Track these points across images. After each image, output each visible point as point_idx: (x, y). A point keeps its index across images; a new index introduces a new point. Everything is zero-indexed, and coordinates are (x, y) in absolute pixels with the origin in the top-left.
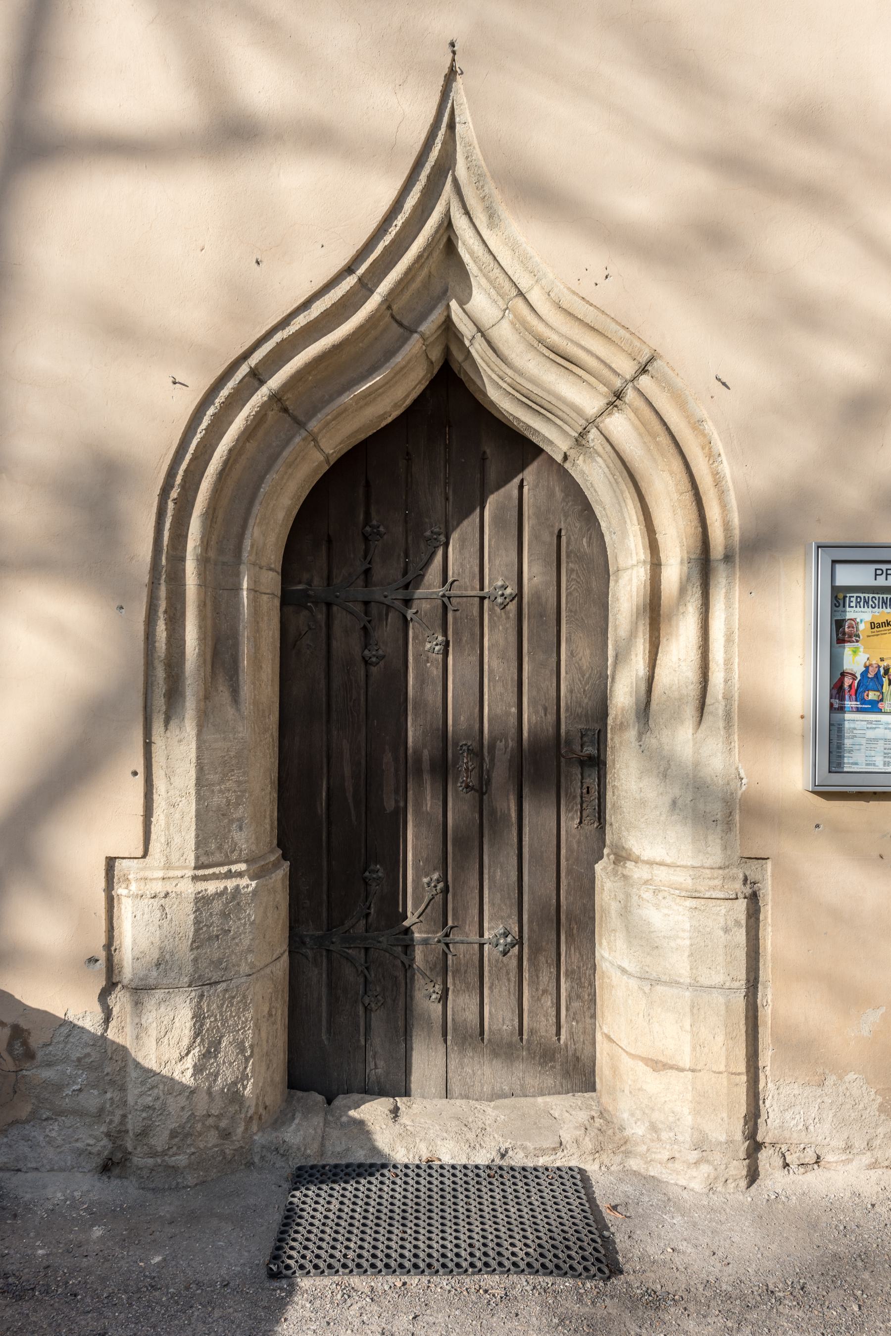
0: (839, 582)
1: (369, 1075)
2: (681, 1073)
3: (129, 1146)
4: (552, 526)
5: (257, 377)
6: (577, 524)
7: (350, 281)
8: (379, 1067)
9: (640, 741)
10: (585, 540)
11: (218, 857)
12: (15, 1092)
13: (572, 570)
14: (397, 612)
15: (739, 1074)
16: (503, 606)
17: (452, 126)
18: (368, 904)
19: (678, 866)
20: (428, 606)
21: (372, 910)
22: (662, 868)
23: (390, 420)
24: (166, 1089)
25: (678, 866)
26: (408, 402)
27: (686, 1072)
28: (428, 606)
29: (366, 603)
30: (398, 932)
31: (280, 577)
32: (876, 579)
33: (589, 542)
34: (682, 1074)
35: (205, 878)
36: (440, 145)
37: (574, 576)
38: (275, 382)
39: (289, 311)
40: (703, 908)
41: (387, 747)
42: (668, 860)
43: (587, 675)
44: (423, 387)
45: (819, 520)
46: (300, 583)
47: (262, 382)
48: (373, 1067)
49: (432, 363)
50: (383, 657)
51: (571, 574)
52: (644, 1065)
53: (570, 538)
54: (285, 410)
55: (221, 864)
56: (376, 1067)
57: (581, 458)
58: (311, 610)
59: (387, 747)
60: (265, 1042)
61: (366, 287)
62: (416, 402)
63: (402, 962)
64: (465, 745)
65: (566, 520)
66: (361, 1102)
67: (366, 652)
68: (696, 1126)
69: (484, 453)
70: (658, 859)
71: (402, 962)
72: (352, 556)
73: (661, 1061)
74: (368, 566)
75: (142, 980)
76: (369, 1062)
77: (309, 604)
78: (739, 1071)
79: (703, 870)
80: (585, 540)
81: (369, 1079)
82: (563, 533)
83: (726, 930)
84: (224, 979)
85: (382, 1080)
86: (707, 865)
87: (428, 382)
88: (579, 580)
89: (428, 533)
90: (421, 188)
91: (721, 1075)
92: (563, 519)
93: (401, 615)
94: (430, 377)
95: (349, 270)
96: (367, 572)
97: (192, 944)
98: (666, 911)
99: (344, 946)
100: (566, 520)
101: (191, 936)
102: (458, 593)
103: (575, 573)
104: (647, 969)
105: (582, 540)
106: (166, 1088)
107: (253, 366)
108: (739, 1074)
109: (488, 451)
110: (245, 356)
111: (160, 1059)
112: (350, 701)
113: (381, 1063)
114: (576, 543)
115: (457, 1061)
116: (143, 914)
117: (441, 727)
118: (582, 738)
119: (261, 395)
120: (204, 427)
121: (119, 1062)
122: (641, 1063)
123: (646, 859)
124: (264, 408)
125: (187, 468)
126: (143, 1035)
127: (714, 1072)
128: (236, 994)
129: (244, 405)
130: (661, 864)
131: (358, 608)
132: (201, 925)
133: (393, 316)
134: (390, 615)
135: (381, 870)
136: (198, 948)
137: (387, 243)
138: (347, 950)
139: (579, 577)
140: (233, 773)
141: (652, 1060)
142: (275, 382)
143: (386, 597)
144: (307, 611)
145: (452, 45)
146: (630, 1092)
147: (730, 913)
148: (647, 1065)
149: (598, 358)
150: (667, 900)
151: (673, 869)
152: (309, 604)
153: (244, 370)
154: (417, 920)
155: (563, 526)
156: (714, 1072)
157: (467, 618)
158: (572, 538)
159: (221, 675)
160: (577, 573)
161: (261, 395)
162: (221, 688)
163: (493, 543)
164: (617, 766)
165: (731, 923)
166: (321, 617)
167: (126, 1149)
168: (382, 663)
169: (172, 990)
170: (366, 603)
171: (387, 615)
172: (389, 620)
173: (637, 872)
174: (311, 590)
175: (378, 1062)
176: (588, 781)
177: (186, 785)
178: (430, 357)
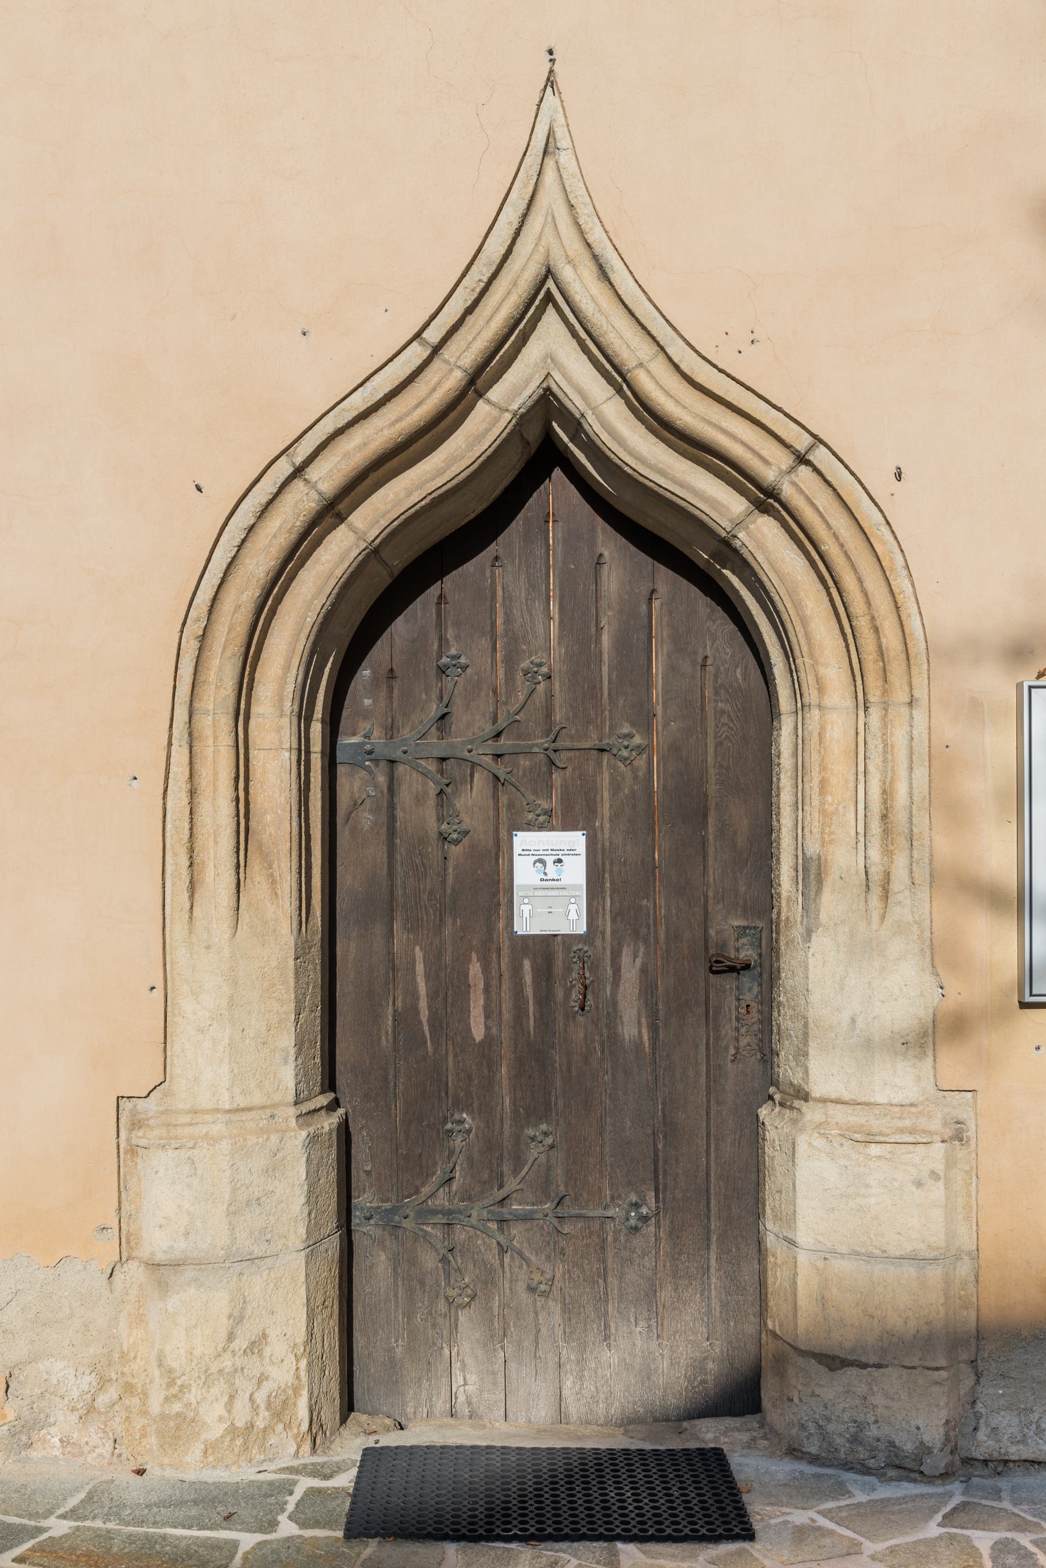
1: (456, 1393)
2: (863, 1370)
4: (695, 653)
6: (728, 650)
8: (469, 1382)
10: (739, 671)
13: (723, 712)
14: (486, 772)
18: (451, 1165)
19: (859, 1104)
20: (527, 763)
22: (839, 1106)
25: (859, 1104)
27: (869, 1369)
28: (527, 763)
30: (492, 1202)
33: (745, 674)
34: (865, 1372)
37: (725, 720)
40: (888, 1156)
41: (474, 956)
42: (846, 1096)
46: (354, 734)
48: (462, 1383)
49: (528, 444)
50: (466, 833)
51: (721, 716)
52: (816, 1364)
53: (719, 668)
56: (465, 1384)
58: (371, 772)
59: (474, 956)
63: (498, 1243)
65: (713, 644)
66: (525, 826)
67: (444, 826)
69: (601, 555)
71: (498, 1243)
72: (424, 697)
73: (839, 1357)
74: (446, 710)
75: (165, 1252)
77: (367, 763)
79: (890, 1108)
80: (739, 671)
82: (709, 662)
85: (474, 1400)
86: (895, 1101)
88: (731, 725)
92: (709, 643)
93: (491, 775)
94: (525, 458)
98: (843, 1162)
99: (420, 1221)
100: (713, 644)
101: (227, 1197)
102: (568, 744)
103: (726, 716)
105: (735, 670)
107: (297, 464)
109: (606, 553)
111: (191, 1353)
112: (424, 892)
113: (472, 1378)
114: (727, 675)
116: (167, 1169)
123: (818, 1095)
130: (838, 1102)
131: (432, 767)
134: (476, 776)
135: (469, 1119)
139: (732, 720)
140: (274, 989)
141: (826, 1356)
144: (364, 772)
145: (551, 52)
146: (801, 1400)
147: (925, 1162)
148: (820, 1363)
149: (743, 443)
150: (844, 1148)
151: (852, 1107)
152: (367, 763)
154: (518, 1187)
155: (709, 652)
157: (580, 779)
158: (722, 668)
159: (258, 861)
160: (729, 716)
162: (257, 879)
163: (614, 677)
164: (783, 975)
166: (382, 779)
168: (466, 841)
169: (204, 1266)
171: (472, 776)
173: (812, 1113)
174: (368, 743)
175: (468, 1376)
176: (748, 997)
177: (217, 1004)
178: (526, 436)
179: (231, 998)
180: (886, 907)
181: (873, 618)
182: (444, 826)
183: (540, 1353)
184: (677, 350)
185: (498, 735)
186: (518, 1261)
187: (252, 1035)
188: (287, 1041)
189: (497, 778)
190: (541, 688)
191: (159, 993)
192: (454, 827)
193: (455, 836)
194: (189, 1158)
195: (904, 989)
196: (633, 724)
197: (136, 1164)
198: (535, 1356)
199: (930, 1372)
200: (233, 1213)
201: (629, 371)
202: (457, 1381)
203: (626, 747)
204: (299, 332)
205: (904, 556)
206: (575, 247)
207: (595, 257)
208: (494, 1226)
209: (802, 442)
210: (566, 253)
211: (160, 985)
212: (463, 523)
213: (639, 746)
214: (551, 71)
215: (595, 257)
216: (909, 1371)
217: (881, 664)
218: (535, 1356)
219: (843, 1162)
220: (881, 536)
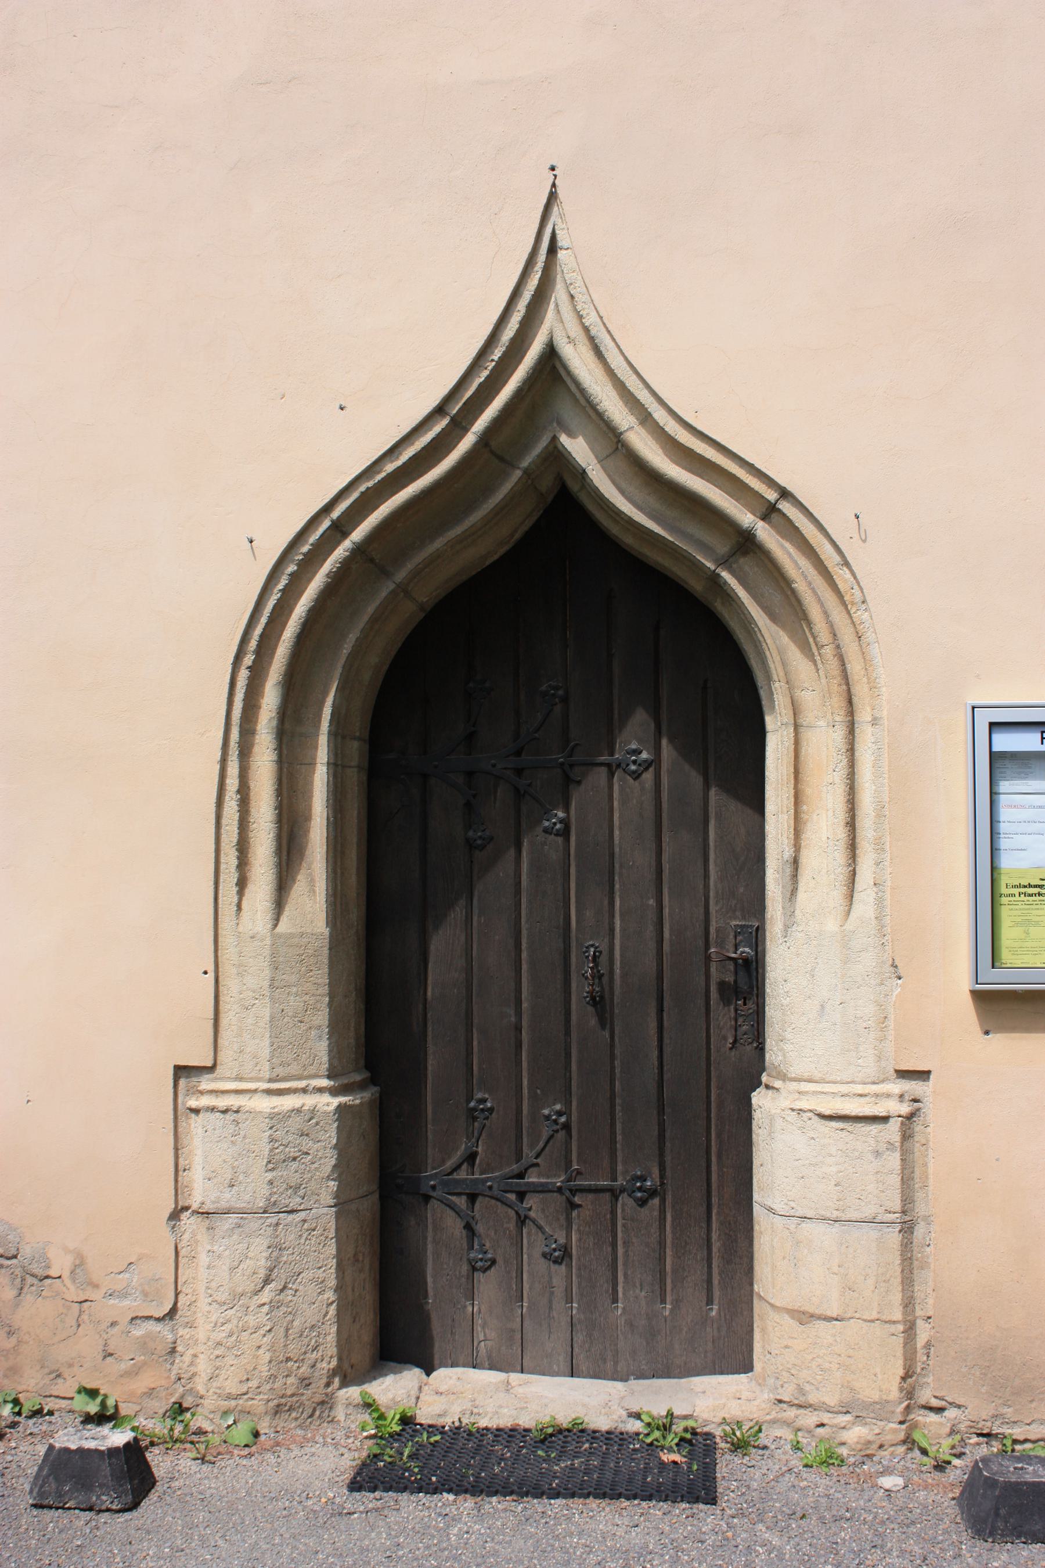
0: (996, 748)
1: (477, 1348)
3: (201, 1389)
5: (340, 529)
7: (440, 425)
9: (786, 937)
11: (294, 1069)
12: (79, 1326)
15: (894, 1322)
16: (636, 775)
17: (553, 249)
21: (480, 1149)
23: (496, 557)
24: (240, 1325)
26: (518, 536)
29: (470, 774)
31: (367, 746)
32: (1042, 743)
35: (280, 1092)
36: (540, 273)
38: (358, 534)
39: (374, 459)
43: (742, 859)
44: (535, 518)
45: (978, 676)
47: (345, 535)
50: (491, 839)
54: (372, 560)
55: (300, 1078)
57: (719, 600)
60: (350, 1289)
61: (459, 426)
62: (527, 535)
64: (592, 946)
67: (471, 833)
68: (846, 1384)
70: (806, 1075)
76: (478, 1334)
77: (402, 777)
78: (895, 1319)
81: (478, 1352)
83: (877, 1154)
84: (302, 1208)
87: (541, 512)
89: (544, 688)
90: (519, 319)
91: (873, 1324)
95: (440, 410)
96: (471, 737)
97: (267, 1165)
104: (793, 1204)
106: (241, 1323)
108: (894, 1322)
110: (327, 509)
111: (234, 1291)
115: (585, 1334)
117: (561, 923)
118: (735, 937)
119: (341, 551)
120: (281, 588)
121: (189, 1296)
122: (786, 1317)
123: (793, 1075)
124: (346, 565)
125: (262, 633)
126: (344, 529)
127: (865, 1320)
128: (316, 1227)
129: (325, 560)
132: (276, 1145)
133: (492, 452)
136: (272, 1170)
137: (482, 379)
138: (450, 1197)
142: (358, 534)
143: (494, 766)
148: (793, 1318)
152: (402, 777)
153: (326, 524)
156: (865, 1320)
161: (341, 551)
165: (882, 1147)
167: (198, 1392)
170: (470, 774)
172: (498, 794)
179: (273, 980)
180: (851, 904)
181: (838, 647)
182: (471, 833)
183: (554, 1314)
184: (660, 415)
185: (518, 753)
186: (534, 1229)
187: (290, 1014)
188: (322, 1018)
189: (517, 790)
190: (558, 709)
191: (211, 975)
192: (479, 834)
193: (479, 842)
194: (234, 1121)
195: (867, 978)
196: (640, 741)
197: (190, 1125)
198: (549, 1316)
199: (887, 1326)
200: (272, 1165)
201: (621, 433)
202: (478, 1337)
203: (634, 762)
204: (338, 407)
205: (862, 592)
206: (575, 331)
207: (592, 339)
208: (512, 1197)
209: (771, 496)
210: (567, 333)
211: (211, 968)
212: (488, 563)
213: (645, 761)
214: (554, 185)
215: (592, 339)
216: (869, 1324)
217: (844, 687)
218: (549, 1316)
219: (812, 1134)
220: (842, 576)
